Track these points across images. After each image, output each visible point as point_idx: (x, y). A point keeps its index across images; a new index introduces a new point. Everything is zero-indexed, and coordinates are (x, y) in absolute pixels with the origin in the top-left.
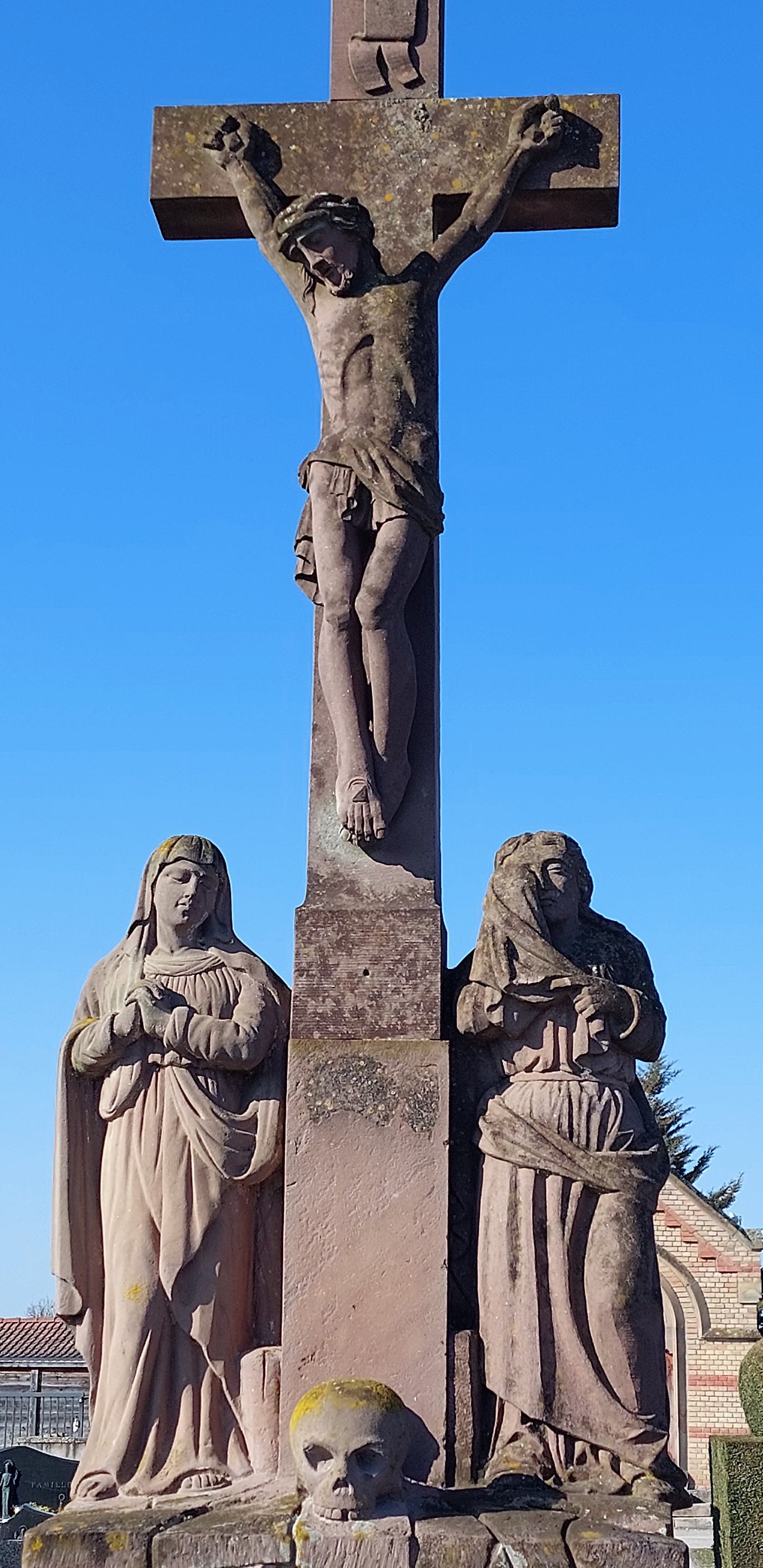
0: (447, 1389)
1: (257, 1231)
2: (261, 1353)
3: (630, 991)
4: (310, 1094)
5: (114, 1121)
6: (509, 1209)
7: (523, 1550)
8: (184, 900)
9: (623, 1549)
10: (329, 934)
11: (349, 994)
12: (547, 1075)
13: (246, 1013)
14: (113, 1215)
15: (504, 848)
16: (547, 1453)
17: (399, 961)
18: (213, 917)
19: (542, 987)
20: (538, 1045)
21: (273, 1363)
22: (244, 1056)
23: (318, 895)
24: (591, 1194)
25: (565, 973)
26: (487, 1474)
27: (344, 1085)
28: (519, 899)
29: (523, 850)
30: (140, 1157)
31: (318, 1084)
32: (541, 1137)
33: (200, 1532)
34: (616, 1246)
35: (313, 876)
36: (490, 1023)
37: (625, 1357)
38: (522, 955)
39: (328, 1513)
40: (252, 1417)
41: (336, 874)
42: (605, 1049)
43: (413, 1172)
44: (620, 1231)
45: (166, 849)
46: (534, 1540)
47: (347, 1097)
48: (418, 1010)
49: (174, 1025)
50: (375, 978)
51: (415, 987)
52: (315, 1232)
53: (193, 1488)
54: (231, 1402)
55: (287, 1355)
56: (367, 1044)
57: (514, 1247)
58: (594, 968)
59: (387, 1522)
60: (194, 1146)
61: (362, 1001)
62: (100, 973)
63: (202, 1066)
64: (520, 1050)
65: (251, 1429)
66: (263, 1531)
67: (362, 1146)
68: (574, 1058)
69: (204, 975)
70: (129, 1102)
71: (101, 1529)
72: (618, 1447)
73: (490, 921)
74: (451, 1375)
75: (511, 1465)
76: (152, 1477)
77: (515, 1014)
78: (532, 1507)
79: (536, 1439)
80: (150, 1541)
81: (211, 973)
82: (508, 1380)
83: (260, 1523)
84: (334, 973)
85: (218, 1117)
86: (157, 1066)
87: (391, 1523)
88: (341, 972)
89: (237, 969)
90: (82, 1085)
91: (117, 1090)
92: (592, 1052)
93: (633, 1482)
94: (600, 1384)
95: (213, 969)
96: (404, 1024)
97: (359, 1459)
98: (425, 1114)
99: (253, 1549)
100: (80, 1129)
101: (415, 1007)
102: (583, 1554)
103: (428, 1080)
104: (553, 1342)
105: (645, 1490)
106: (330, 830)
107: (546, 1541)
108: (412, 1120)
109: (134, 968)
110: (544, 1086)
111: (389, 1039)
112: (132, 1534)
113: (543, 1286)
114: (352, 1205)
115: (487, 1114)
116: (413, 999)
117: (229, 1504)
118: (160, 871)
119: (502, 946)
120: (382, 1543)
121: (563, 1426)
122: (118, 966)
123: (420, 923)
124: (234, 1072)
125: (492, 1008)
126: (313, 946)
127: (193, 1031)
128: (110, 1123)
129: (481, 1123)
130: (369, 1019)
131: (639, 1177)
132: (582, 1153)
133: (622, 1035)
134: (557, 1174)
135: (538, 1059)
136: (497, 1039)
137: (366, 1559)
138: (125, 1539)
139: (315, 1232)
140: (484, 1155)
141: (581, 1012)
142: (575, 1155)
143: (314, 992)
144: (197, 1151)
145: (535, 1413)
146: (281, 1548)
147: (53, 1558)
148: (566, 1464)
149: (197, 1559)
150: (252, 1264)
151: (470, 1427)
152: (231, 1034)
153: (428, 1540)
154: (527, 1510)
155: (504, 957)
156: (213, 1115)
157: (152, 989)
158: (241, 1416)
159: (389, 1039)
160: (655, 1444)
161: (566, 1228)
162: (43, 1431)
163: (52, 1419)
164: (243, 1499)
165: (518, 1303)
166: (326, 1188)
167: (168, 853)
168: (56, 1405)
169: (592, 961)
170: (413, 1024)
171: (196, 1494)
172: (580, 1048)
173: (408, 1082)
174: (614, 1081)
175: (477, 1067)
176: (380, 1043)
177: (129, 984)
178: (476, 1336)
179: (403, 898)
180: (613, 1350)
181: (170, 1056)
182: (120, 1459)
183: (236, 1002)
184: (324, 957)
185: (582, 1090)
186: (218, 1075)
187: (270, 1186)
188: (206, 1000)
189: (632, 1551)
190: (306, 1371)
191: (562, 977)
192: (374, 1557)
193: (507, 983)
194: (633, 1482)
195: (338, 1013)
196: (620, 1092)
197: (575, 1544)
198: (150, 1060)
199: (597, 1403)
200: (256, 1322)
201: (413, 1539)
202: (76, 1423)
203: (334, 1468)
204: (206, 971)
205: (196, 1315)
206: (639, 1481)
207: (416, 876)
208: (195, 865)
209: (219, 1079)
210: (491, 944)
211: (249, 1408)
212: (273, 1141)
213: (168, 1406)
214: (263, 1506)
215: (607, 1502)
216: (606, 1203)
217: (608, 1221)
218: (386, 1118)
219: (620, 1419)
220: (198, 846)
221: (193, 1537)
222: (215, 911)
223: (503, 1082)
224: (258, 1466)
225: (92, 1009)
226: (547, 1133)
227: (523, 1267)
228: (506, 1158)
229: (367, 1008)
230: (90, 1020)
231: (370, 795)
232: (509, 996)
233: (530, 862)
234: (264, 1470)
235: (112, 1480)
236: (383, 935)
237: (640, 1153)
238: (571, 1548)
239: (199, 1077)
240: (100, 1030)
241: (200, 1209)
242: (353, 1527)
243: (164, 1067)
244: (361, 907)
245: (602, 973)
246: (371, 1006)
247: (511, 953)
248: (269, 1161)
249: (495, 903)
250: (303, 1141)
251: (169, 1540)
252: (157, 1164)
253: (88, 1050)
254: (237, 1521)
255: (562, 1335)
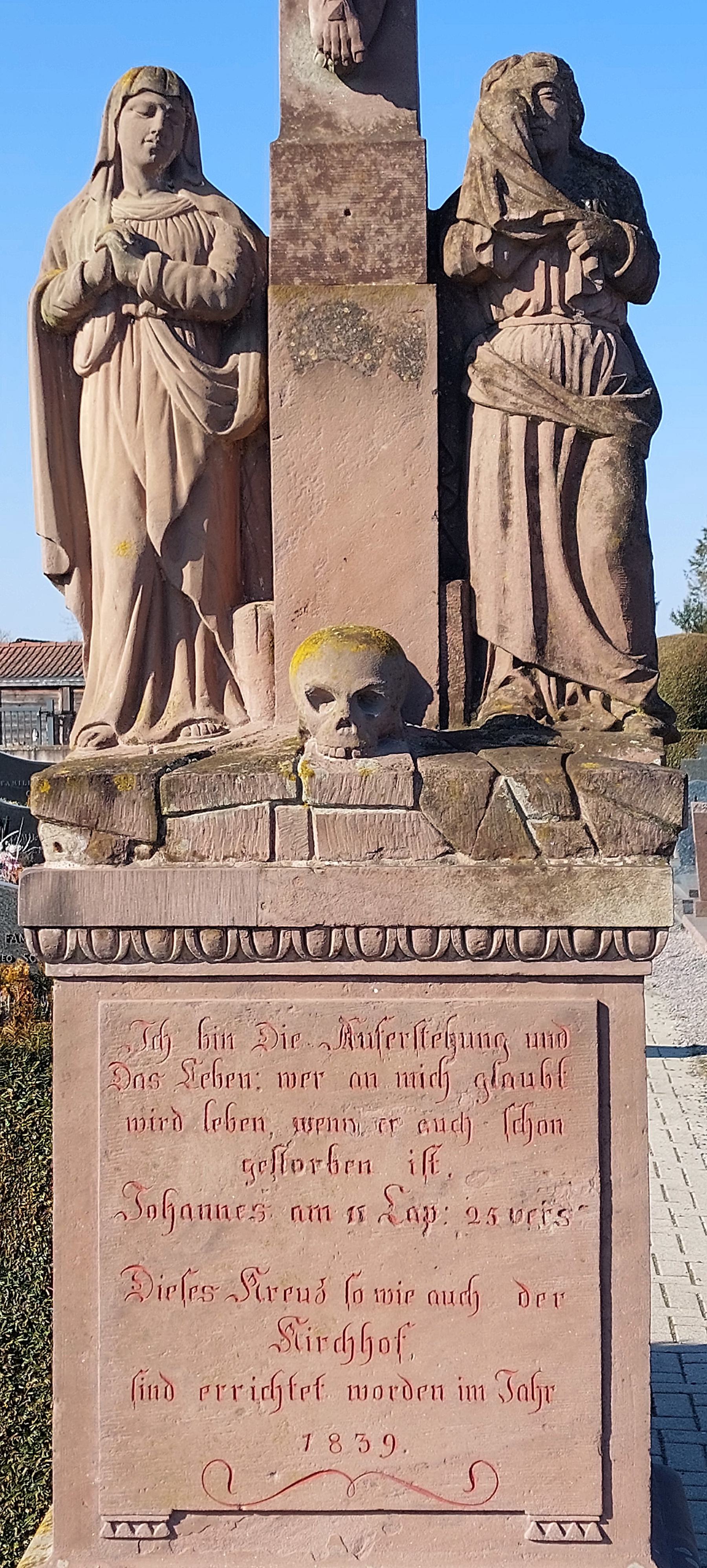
0: (439, 637)
1: (242, 489)
2: (253, 607)
3: (625, 226)
4: (293, 344)
5: (91, 377)
6: (500, 458)
7: (524, 781)
8: (151, 136)
9: (624, 778)
10: (308, 170)
11: (330, 237)
12: (538, 319)
13: (222, 259)
14: (95, 473)
15: (491, 73)
16: (539, 695)
17: (382, 199)
18: (182, 156)
19: (533, 223)
20: (528, 286)
21: (266, 617)
22: (223, 304)
23: (293, 129)
24: (584, 440)
25: (559, 208)
26: (480, 716)
27: (328, 334)
28: (509, 127)
29: (511, 74)
30: (120, 412)
31: (300, 333)
32: (533, 383)
33: (206, 772)
34: (610, 490)
35: (287, 108)
36: (480, 264)
37: (618, 599)
38: (512, 188)
39: (332, 752)
40: (247, 669)
41: (311, 106)
42: (599, 288)
43: (401, 422)
44: (614, 475)
45: (129, 80)
46: (536, 772)
47: (331, 347)
48: (403, 252)
49: (148, 271)
50: (357, 219)
51: (399, 227)
52: (303, 486)
53: (192, 736)
54: (225, 656)
55: (279, 608)
56: (351, 290)
57: (505, 497)
58: (587, 203)
59: (390, 759)
60: (175, 401)
61: (344, 244)
62: (66, 220)
63: (179, 316)
64: (510, 293)
65: (246, 680)
66: (269, 770)
67: (349, 397)
68: (567, 298)
69: (175, 219)
70: (104, 356)
71: (109, 771)
72: (609, 686)
73: (478, 153)
74: (443, 623)
75: (504, 707)
76: (151, 727)
77: (506, 253)
78: (527, 743)
79: (527, 681)
80: (158, 782)
81: (182, 217)
82: (500, 626)
83: (265, 763)
84: (314, 214)
85: (198, 370)
86: (132, 318)
87: (394, 760)
88: (321, 213)
89: (210, 213)
90: (54, 340)
91: (91, 343)
92: (585, 292)
93: (624, 718)
94: (592, 627)
95: (185, 212)
96: (389, 268)
97: (361, 700)
98: (412, 363)
99: (260, 786)
100: (55, 387)
101: (400, 248)
102: (584, 784)
103: (415, 326)
104: (545, 588)
105: (637, 726)
106: (304, 56)
107: (548, 772)
108: (400, 368)
109: (101, 213)
110: (535, 330)
111: (374, 284)
112: (139, 775)
113: (535, 533)
114: (341, 458)
115: (476, 361)
116: (398, 240)
117: (231, 747)
118: (123, 105)
119: (492, 179)
120: (386, 778)
121: (555, 668)
122: (83, 212)
123: (404, 156)
124: (212, 324)
125: (482, 247)
126: (291, 184)
127: (168, 278)
128: (85, 379)
129: (470, 370)
130: (352, 263)
131: (633, 420)
132: (575, 397)
133: (617, 273)
134: (550, 420)
135: (529, 301)
136: (486, 282)
137: (371, 793)
138: (133, 780)
139: (303, 486)
140: (474, 404)
141: (574, 250)
142: (567, 401)
143: (293, 235)
144: (179, 406)
145: (527, 656)
146: (288, 785)
147: (62, 799)
148: (558, 705)
149: (205, 797)
150: (239, 521)
151: (463, 673)
152: (208, 281)
153: (431, 774)
154: (524, 746)
155: (494, 191)
156: (193, 368)
157: (122, 233)
158: (235, 668)
159: (374, 284)
160: (646, 682)
161: (559, 474)
162: (6, 742)
163: (14, 731)
164: (245, 743)
165: (510, 551)
166: (313, 441)
167: (131, 85)
168: (16, 719)
169: (583, 196)
170: (398, 267)
171: (196, 742)
172: (573, 287)
173: (395, 329)
174: (607, 324)
175: (465, 310)
176: (364, 289)
177: (97, 229)
178: (467, 586)
179: (384, 130)
180: (605, 593)
181: (145, 306)
182: (118, 711)
183: (211, 248)
184: (302, 197)
185: (574, 333)
186: (195, 325)
187: (258, 435)
188: (179, 246)
189: (632, 779)
190: (300, 622)
191: (555, 211)
192: (379, 792)
193: (498, 219)
194: (624, 718)
195: (319, 257)
196: (613, 334)
197: (577, 774)
198: (124, 311)
199: (589, 645)
200: (248, 577)
201: (416, 774)
202: (35, 734)
203: (337, 709)
204: (178, 215)
205: (187, 570)
206: (630, 717)
207: (397, 107)
208: (160, 97)
209: (197, 331)
210: (480, 177)
211: (244, 660)
212: (255, 394)
213: (162, 659)
214: (266, 749)
215: (601, 738)
216: (600, 448)
217: (601, 465)
218: (373, 368)
219: (612, 660)
220: (163, 77)
221: (201, 776)
222: (183, 150)
223: (491, 329)
224: (254, 716)
225: (59, 260)
226: (539, 378)
227: (515, 515)
228: (498, 405)
229: (349, 251)
230: (57, 271)
231: (348, 13)
232: (500, 234)
233: (519, 86)
234: (260, 718)
235: (111, 730)
236: (363, 171)
237: (635, 396)
238: (572, 778)
239: (176, 329)
240: (70, 278)
241: (185, 465)
242: (357, 764)
243: (138, 318)
244: (340, 140)
245: (595, 208)
246: (353, 249)
247: (501, 188)
248: (252, 416)
249: (483, 133)
250: (288, 393)
251: (176, 780)
252: (139, 413)
253: (56, 304)
254: (243, 761)
255: (554, 581)
